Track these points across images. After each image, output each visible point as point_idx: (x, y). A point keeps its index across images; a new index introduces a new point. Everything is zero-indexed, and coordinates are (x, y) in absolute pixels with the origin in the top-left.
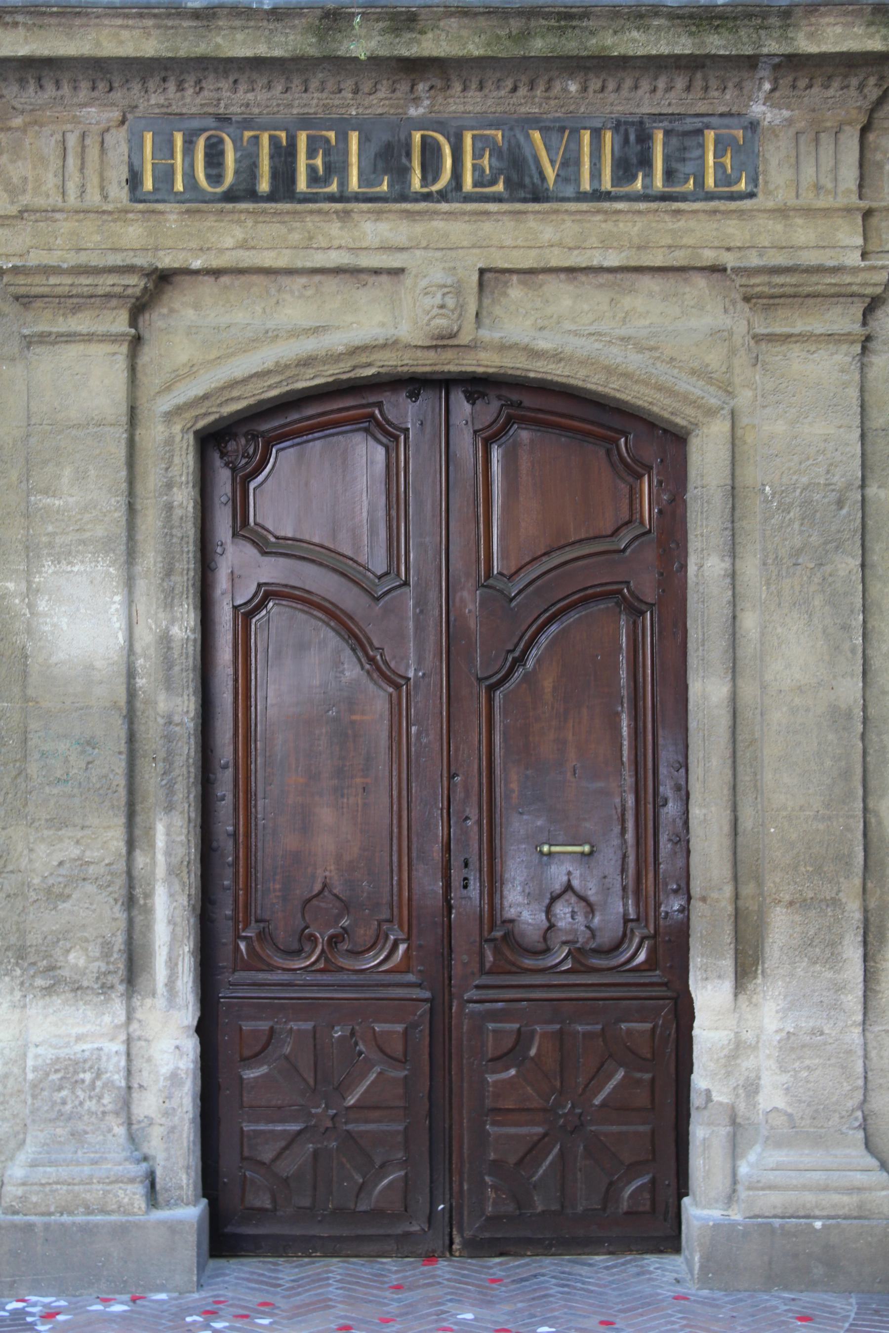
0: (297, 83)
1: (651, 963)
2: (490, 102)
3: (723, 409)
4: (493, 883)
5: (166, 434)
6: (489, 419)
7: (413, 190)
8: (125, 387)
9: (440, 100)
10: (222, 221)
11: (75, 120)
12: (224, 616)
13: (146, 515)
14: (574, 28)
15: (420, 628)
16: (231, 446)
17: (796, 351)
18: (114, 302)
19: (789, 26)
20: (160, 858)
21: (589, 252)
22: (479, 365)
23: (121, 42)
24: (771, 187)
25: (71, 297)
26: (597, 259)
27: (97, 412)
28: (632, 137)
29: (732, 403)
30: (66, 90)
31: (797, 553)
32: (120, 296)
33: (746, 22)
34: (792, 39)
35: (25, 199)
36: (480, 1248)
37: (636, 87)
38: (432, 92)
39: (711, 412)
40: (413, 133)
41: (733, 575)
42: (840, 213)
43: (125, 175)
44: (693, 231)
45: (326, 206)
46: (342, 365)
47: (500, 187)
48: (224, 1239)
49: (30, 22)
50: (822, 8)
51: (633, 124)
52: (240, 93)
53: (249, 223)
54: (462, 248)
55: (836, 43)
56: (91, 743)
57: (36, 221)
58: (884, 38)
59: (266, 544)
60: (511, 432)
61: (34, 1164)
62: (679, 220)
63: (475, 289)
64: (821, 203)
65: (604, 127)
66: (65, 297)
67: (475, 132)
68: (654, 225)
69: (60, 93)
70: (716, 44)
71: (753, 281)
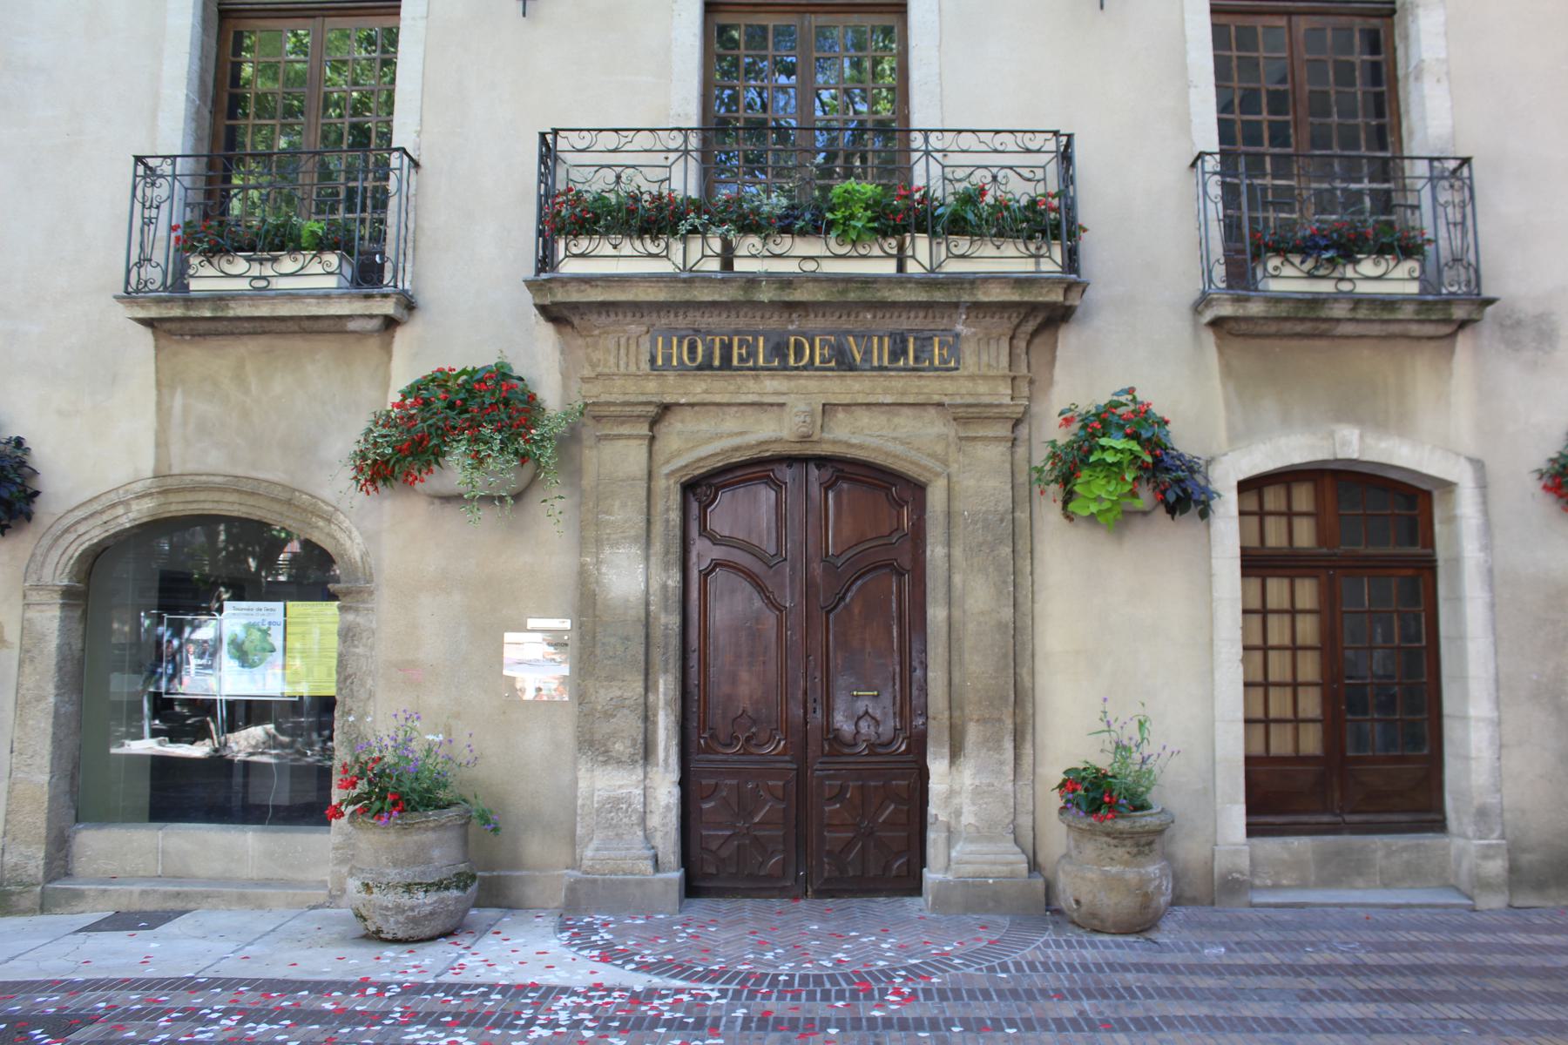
0: (733, 313)
1: (908, 751)
4: (829, 711)
11: (625, 331)
15: (792, 581)
20: (661, 696)
26: (881, 399)
30: (621, 317)
31: (980, 545)
35: (599, 370)
36: (821, 894)
39: (938, 475)
41: (949, 556)
47: (833, 364)
48: (693, 888)
59: (715, 540)
61: (597, 850)
64: (991, 373)
70: (939, 296)
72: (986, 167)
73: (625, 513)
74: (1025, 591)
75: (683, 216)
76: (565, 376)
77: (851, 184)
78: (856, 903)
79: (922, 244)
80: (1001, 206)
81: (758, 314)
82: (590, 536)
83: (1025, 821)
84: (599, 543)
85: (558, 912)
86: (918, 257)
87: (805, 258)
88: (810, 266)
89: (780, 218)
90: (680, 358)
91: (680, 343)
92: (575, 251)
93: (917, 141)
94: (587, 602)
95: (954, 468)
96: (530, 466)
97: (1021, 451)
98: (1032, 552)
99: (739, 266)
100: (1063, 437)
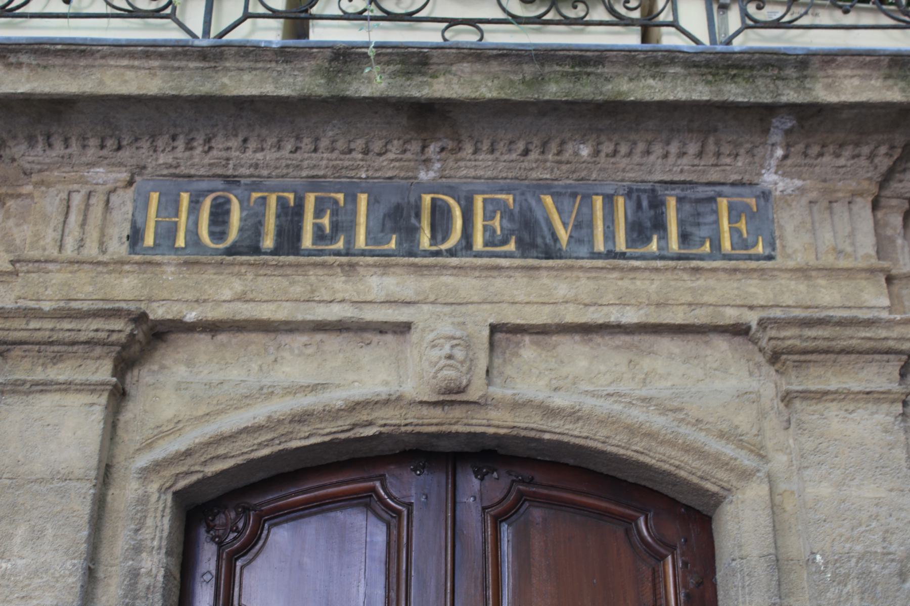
2: (501, 165)
3: (758, 471)
5: (140, 492)
6: (498, 496)
7: (421, 248)
8: (99, 439)
9: (451, 163)
10: (222, 274)
11: (83, 181)
13: (108, 585)
14: (589, 74)
16: (220, 520)
17: (833, 410)
18: (98, 350)
19: (805, 77)
21: (605, 309)
22: (489, 426)
23: (126, 82)
24: (790, 251)
25: (51, 343)
26: (614, 316)
27: (64, 466)
28: (645, 204)
29: (767, 467)
30: (74, 148)
32: (103, 343)
33: (763, 72)
34: (810, 89)
37: (648, 152)
38: (443, 154)
39: (746, 475)
40: (424, 196)
42: (863, 275)
43: (127, 231)
44: (714, 289)
45: (331, 259)
46: (340, 423)
47: (511, 246)
49: (34, 63)
50: (839, 58)
51: (645, 191)
52: (249, 153)
53: (250, 276)
54: (472, 303)
55: (854, 94)
57: (28, 272)
58: (903, 90)
60: (522, 510)
62: (698, 279)
63: (487, 345)
65: (616, 194)
66: (45, 343)
67: (486, 196)
68: (672, 283)
69: (68, 151)
70: (735, 92)
71: (783, 334)
88: (466, 37)
91: (195, 204)
95: (779, 461)
99: (319, 33)
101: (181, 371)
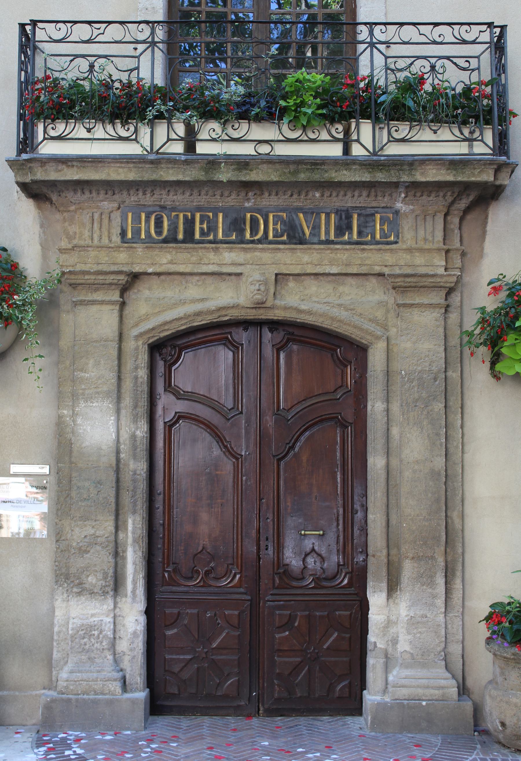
0: (196, 191)
1: (350, 584)
2: (281, 201)
4: (279, 547)
6: (279, 340)
9: (259, 199)
11: (98, 207)
12: (160, 426)
15: (247, 432)
17: (416, 311)
18: (113, 287)
20: (130, 535)
24: (405, 239)
28: (343, 217)
29: (387, 334)
30: (94, 194)
33: (394, 167)
35: (75, 242)
36: (272, 713)
39: (378, 338)
41: (388, 410)
43: (119, 231)
45: (208, 245)
46: (214, 315)
47: (285, 238)
48: (156, 707)
51: (344, 211)
52: (171, 196)
53: (174, 253)
55: (433, 177)
56: (100, 483)
59: (179, 395)
61: (72, 672)
63: (274, 283)
64: (427, 247)
65: (331, 212)
70: (381, 177)
71: (397, 280)
72: (425, 58)
73: (98, 371)
74: (455, 442)
75: (150, 103)
76: (45, 247)
77: (302, 74)
78: (303, 721)
79: (366, 129)
80: (437, 93)
81: (218, 192)
82: (67, 391)
83: (455, 649)
84: (75, 397)
85: (35, 728)
86: (362, 140)
87: (260, 142)
88: (264, 149)
89: (238, 105)
90: (148, 232)
91: (148, 218)
92: (53, 133)
93: (363, 33)
94: (64, 451)
95: (393, 331)
96: (12, 329)
97: (454, 317)
98: (462, 408)
99: (201, 148)
100: (491, 304)
101: (147, 293)
